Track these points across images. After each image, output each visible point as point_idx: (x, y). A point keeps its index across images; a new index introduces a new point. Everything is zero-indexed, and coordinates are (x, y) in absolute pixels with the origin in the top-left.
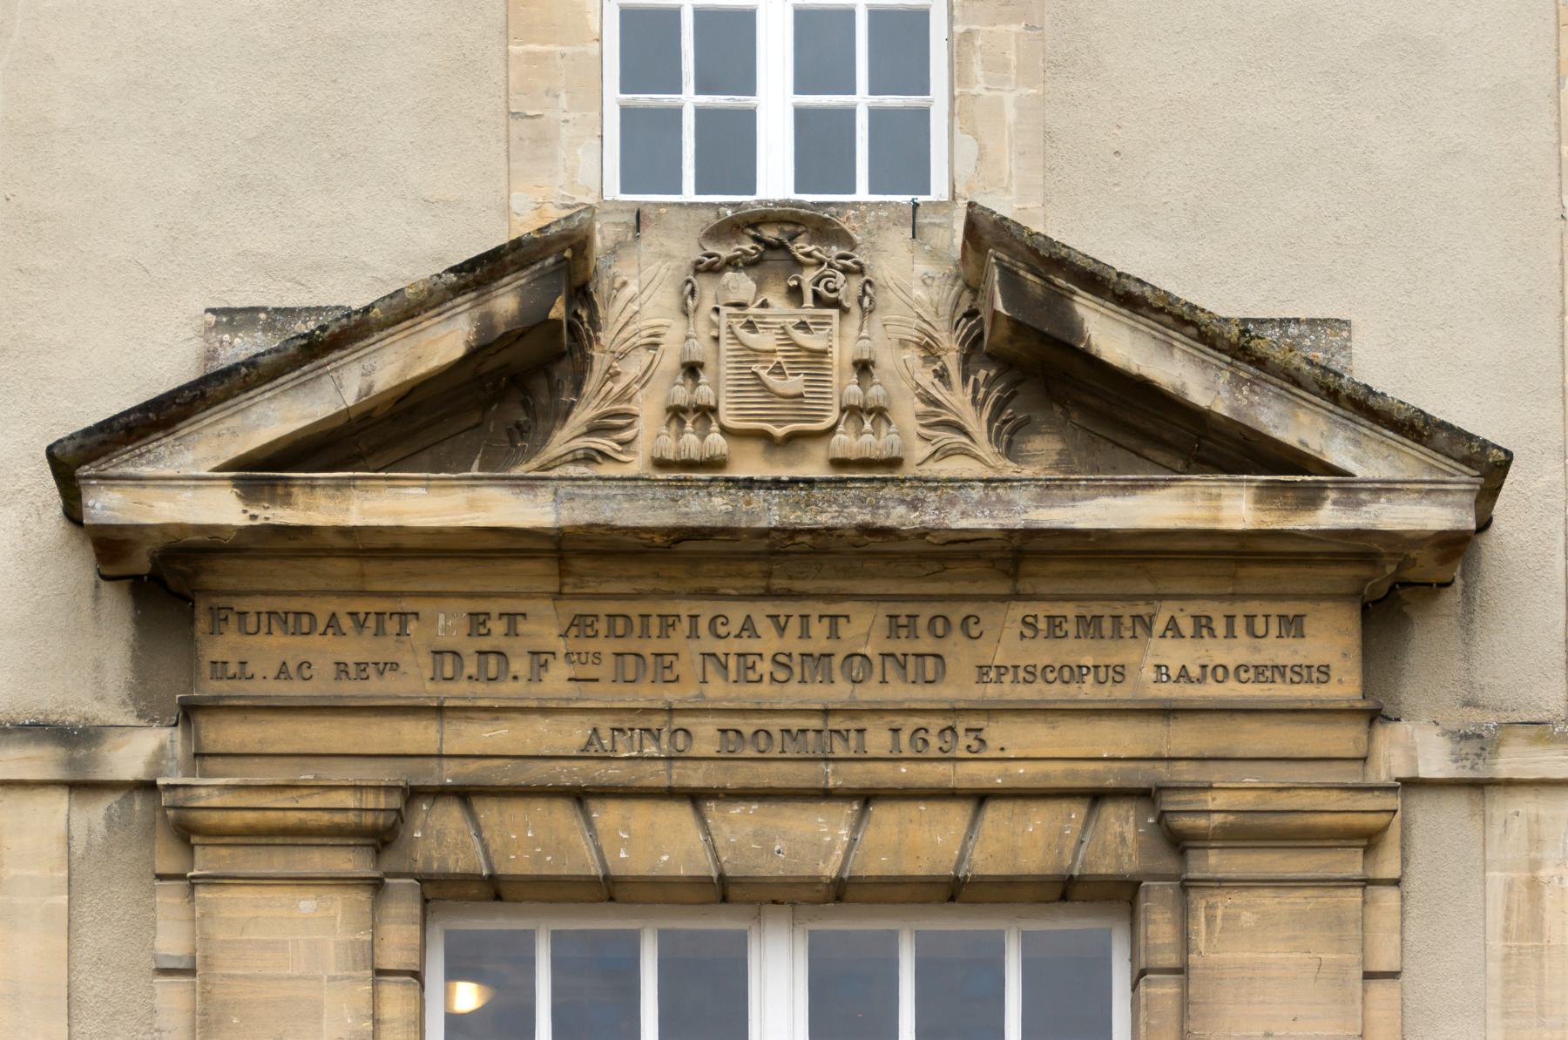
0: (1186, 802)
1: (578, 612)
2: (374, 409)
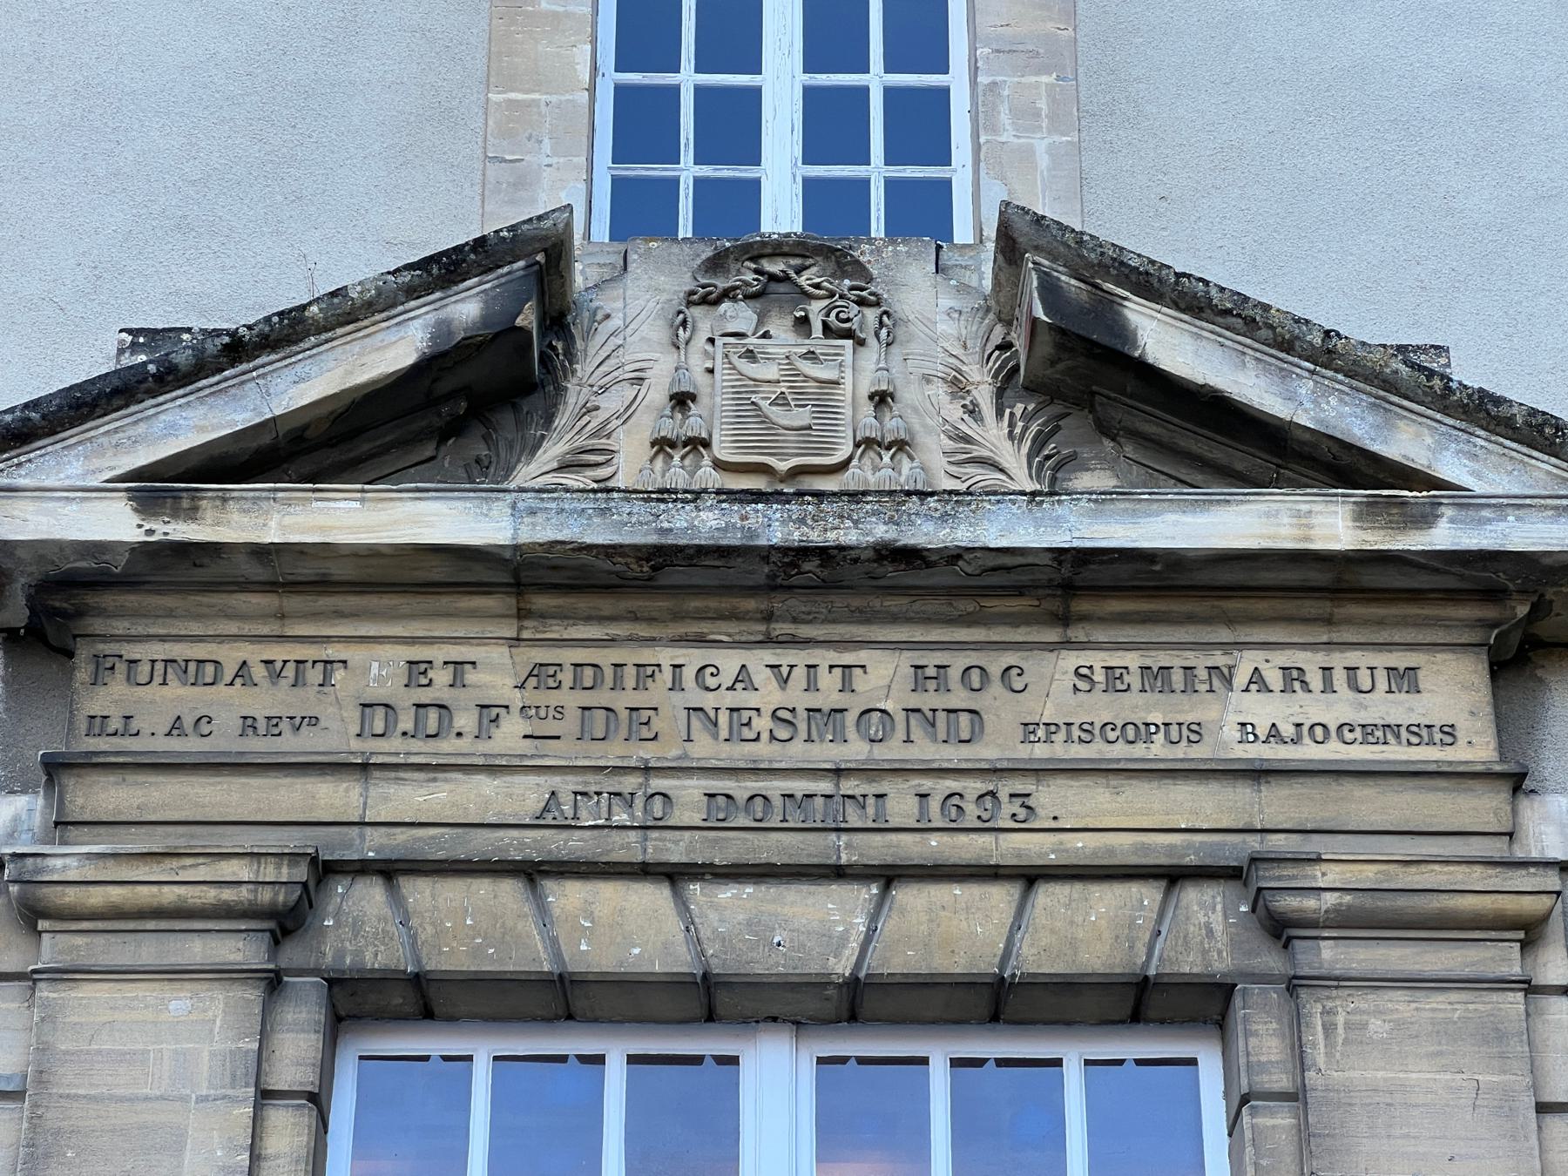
0: (1294, 877)
1: (539, 661)
2: (306, 427)
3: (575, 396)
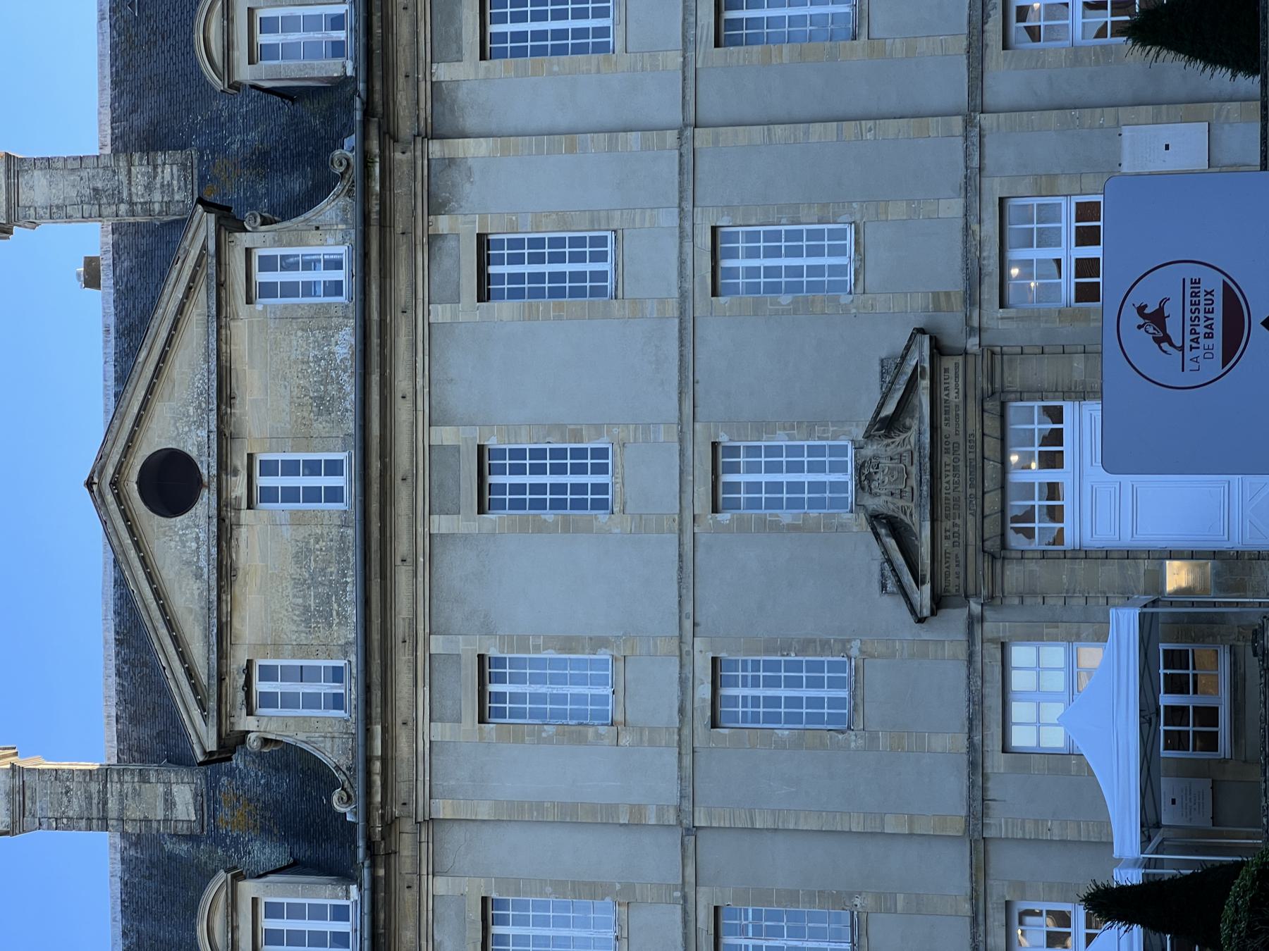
3: (890, 513)
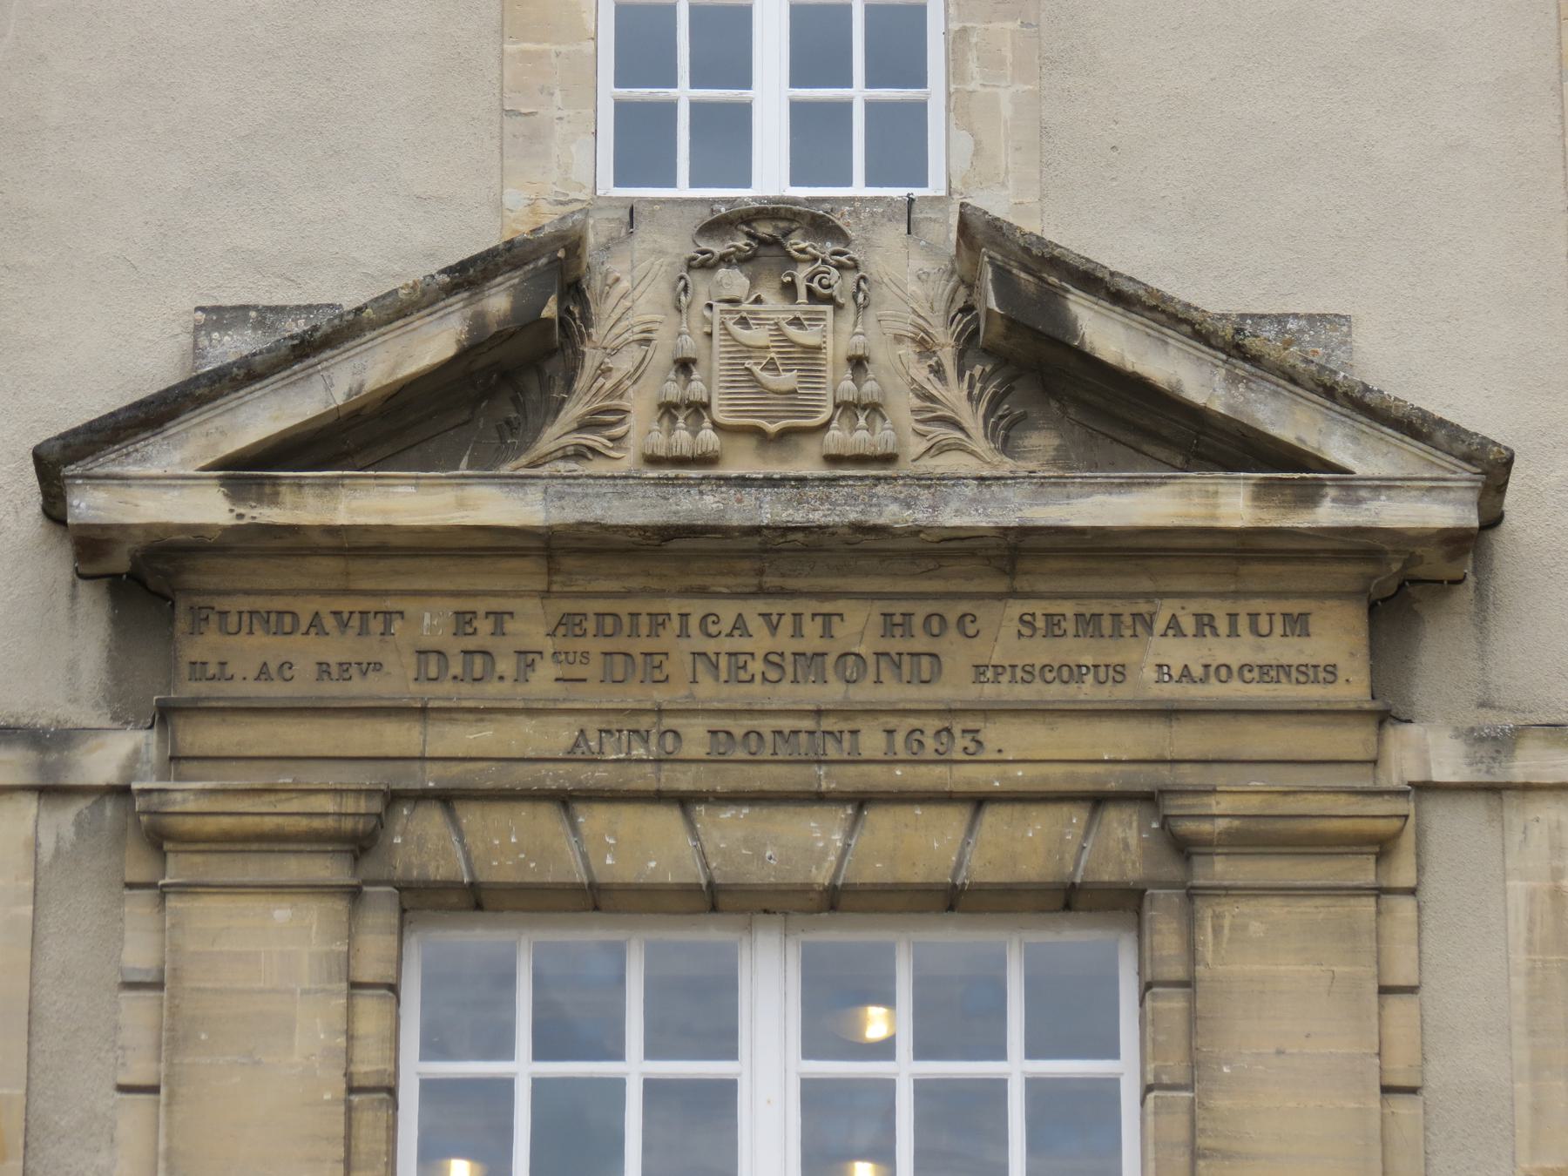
0: (1191, 806)
3: (592, 358)
